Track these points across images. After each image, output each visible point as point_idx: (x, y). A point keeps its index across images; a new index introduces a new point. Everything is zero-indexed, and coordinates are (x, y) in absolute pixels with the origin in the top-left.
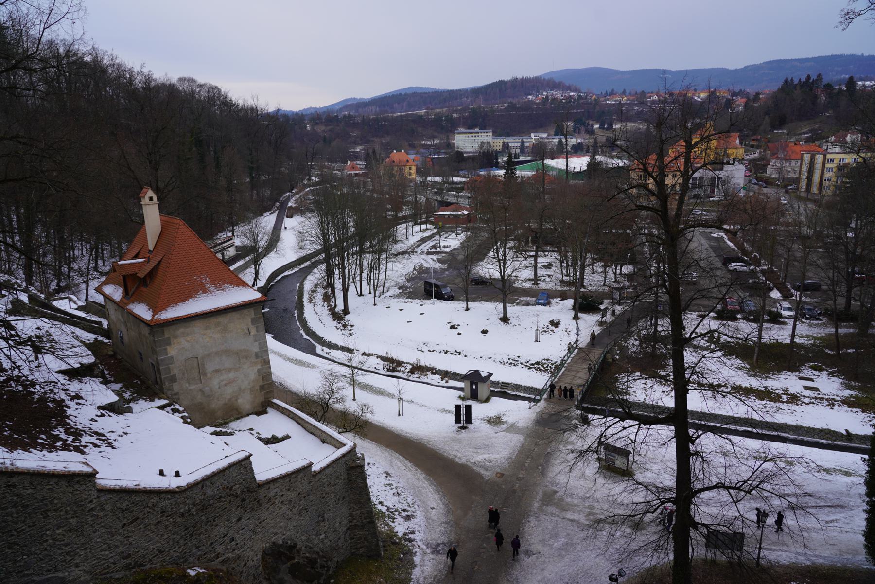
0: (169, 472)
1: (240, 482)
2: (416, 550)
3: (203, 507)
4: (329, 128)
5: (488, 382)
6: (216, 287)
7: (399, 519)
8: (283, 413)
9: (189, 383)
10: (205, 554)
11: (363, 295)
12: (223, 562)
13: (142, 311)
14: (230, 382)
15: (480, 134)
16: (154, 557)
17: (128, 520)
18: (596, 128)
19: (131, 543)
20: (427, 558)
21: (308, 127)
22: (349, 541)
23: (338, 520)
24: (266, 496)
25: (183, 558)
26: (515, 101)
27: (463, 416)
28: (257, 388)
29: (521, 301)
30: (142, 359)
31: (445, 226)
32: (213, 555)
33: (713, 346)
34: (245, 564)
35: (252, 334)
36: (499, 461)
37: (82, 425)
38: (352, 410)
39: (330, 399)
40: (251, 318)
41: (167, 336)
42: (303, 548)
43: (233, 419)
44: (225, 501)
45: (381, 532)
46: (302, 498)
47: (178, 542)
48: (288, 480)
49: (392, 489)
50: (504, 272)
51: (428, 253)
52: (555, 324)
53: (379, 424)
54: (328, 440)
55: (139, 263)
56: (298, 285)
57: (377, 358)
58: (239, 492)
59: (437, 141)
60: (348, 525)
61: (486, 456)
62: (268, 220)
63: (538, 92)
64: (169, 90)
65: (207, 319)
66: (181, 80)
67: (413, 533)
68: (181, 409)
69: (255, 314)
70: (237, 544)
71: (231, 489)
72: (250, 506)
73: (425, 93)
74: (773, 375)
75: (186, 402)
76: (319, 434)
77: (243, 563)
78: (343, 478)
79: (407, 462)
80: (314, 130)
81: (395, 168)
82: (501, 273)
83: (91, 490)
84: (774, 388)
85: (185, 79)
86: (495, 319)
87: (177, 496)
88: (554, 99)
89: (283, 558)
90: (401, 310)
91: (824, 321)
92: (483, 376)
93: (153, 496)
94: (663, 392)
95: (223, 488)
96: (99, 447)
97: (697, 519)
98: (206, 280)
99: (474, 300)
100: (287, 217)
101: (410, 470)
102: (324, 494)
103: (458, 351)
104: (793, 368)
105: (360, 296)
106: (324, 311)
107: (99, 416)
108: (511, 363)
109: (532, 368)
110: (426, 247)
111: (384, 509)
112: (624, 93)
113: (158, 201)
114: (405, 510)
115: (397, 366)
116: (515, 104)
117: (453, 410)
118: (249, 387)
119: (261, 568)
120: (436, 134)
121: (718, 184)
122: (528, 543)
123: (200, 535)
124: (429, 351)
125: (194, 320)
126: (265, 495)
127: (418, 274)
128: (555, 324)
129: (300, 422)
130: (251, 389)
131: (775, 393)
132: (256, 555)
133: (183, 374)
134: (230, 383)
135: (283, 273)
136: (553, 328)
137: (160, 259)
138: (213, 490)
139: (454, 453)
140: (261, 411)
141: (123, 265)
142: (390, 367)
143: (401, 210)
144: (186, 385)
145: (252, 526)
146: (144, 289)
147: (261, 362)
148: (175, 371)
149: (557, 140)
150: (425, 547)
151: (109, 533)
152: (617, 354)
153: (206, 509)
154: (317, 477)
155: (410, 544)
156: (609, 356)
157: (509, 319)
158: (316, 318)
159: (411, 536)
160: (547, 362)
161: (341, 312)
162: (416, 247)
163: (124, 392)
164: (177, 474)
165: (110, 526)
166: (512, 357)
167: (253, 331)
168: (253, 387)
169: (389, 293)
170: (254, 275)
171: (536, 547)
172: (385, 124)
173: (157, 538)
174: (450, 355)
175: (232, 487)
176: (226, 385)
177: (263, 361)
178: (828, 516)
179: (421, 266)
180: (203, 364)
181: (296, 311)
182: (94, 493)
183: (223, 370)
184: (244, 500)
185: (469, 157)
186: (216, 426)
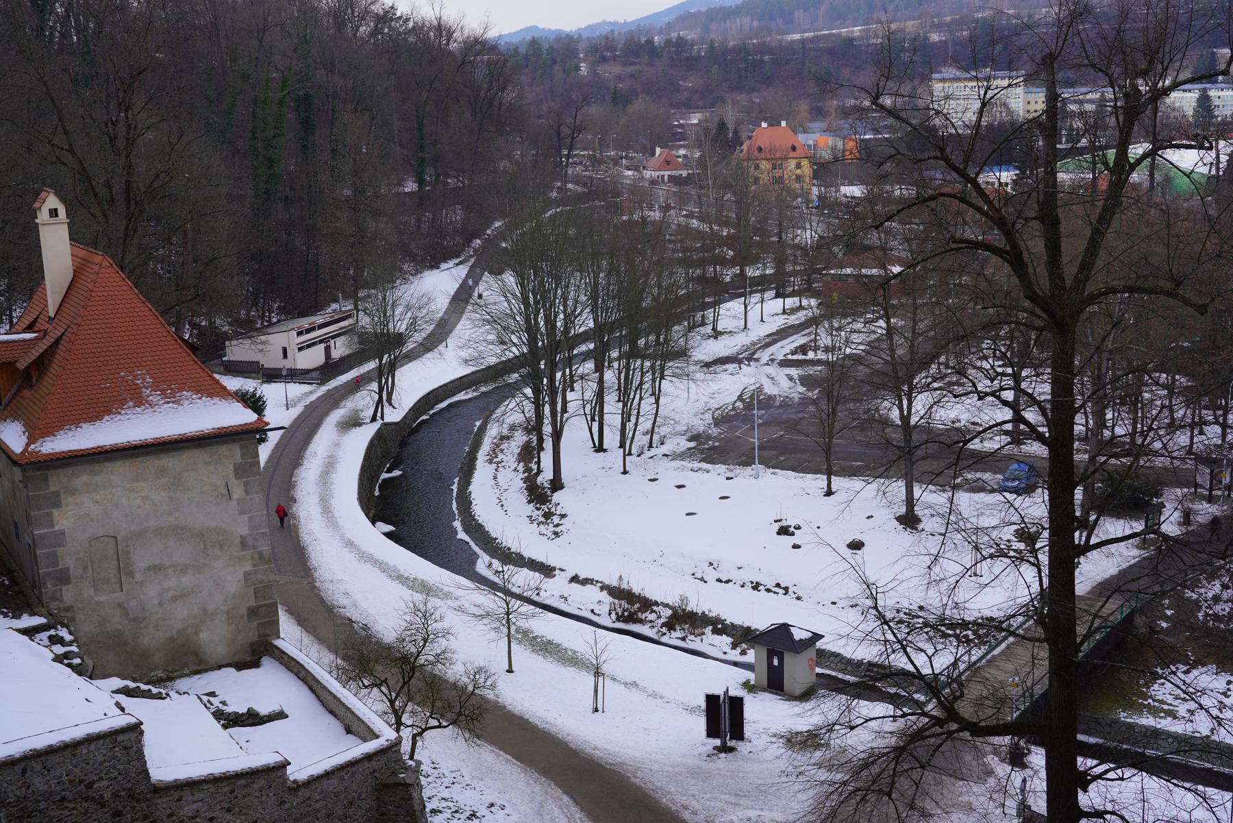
1: (113, 776)
4: (630, 69)
5: (810, 653)
6: (163, 392)
8: (289, 669)
9: (96, 590)
11: (605, 451)
14: (183, 595)
21: (584, 69)
24: (171, 815)
28: (243, 611)
35: (235, 497)
39: (419, 653)
40: (235, 465)
41: (53, 488)
43: (186, 671)
44: (73, 809)
48: (227, 789)
51: (785, 363)
53: (541, 725)
54: (354, 728)
55: (25, 341)
56: (478, 423)
57: (602, 589)
58: (107, 796)
65: (140, 459)
68: (68, 638)
69: (242, 456)
71: (90, 786)
75: (87, 627)
76: (342, 713)
79: (574, 809)
86: (886, 517)
90: (679, 487)
95: (71, 782)
98: (144, 379)
99: (851, 473)
103: (783, 586)
105: (597, 451)
106: (513, 480)
109: (948, 636)
110: (783, 349)
115: (640, 610)
117: (704, 706)
118: (225, 608)
124: (719, 580)
125: (111, 460)
126: (169, 811)
127: (745, 408)
129: (314, 687)
130: (228, 612)
133: (85, 569)
134: (184, 595)
135: (454, 394)
137: (59, 334)
138: (47, 782)
139: (684, 800)
140: (248, 660)
142: (624, 610)
143: (753, 261)
144: (88, 592)
146: (27, 393)
147: (252, 558)
148: (68, 562)
153: (29, 816)
154: (300, 794)
156: (1139, 620)
157: (920, 521)
161: (547, 485)
162: (760, 348)
168: (233, 608)
169: (664, 449)
170: (376, 397)
172: (762, 61)
174: (763, 592)
175: (93, 782)
176: (174, 599)
177: (256, 556)
180: (128, 553)
181: (456, 480)
183: (169, 567)
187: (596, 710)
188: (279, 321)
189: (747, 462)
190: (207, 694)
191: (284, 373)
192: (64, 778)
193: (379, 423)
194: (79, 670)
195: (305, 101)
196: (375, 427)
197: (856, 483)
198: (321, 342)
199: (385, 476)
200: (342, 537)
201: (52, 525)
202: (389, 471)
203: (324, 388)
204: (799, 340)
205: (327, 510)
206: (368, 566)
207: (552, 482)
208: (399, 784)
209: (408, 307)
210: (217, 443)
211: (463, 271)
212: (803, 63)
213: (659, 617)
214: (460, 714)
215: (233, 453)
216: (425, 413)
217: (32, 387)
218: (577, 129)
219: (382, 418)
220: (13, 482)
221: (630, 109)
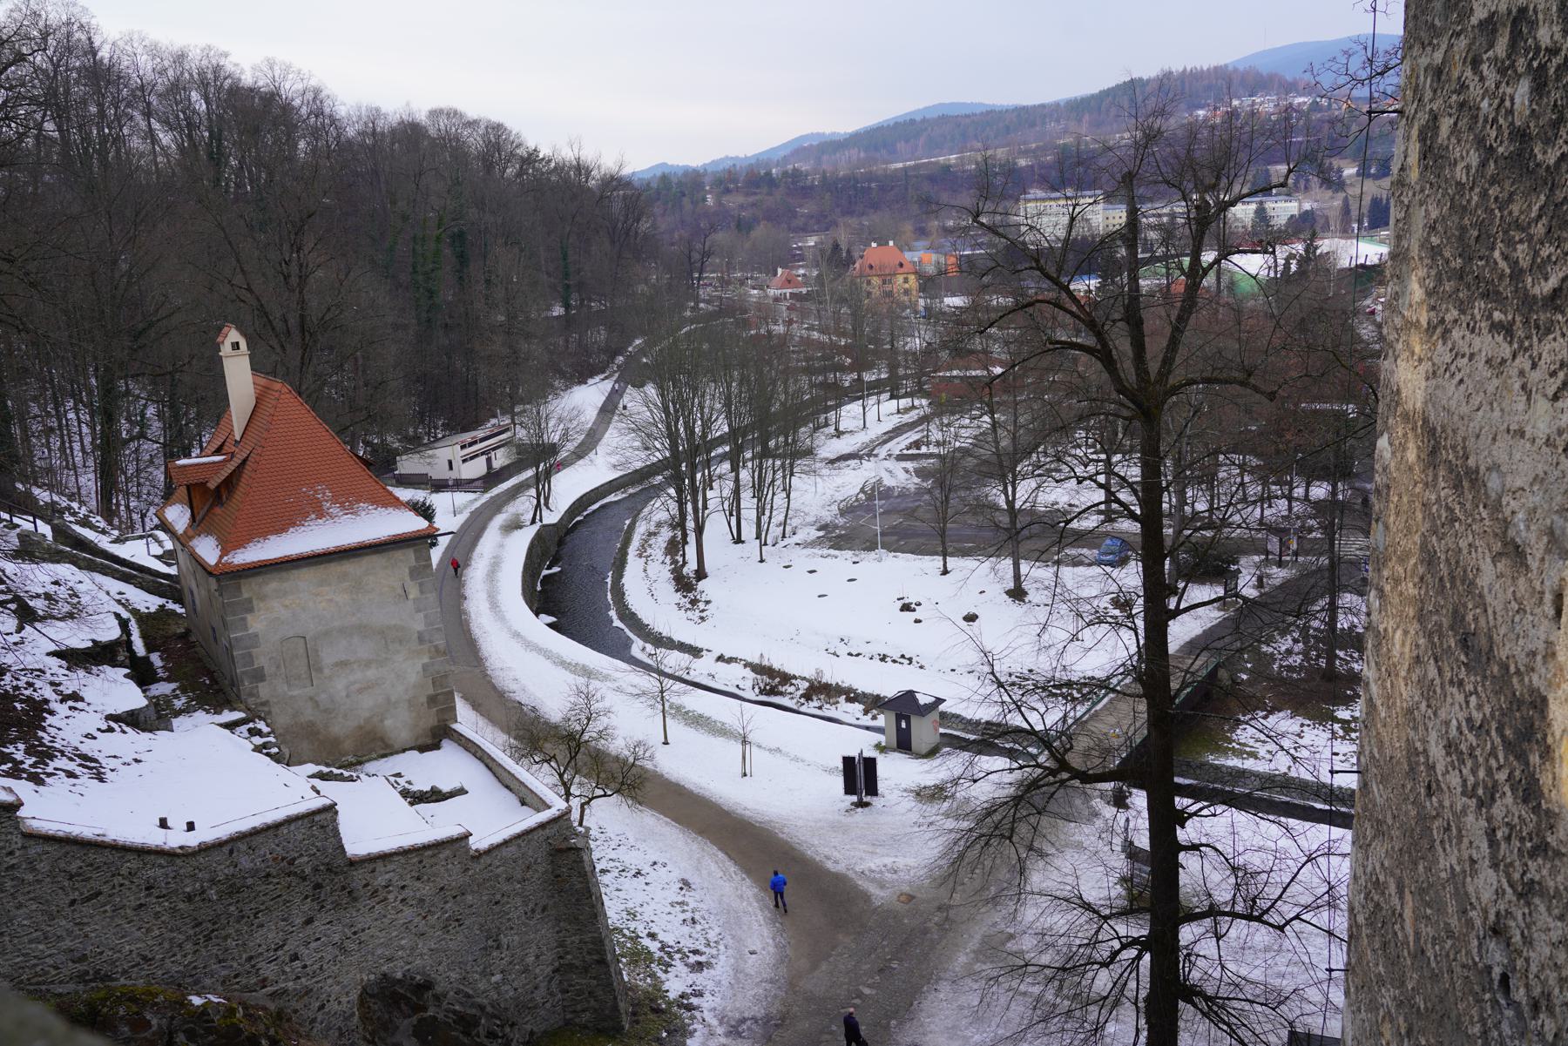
0: (174, 821)
2: (695, 1026)
3: (233, 889)
4: (751, 199)
5: (934, 716)
7: (679, 966)
9: (288, 683)
10: (236, 976)
11: (743, 542)
12: (273, 995)
13: (208, 550)
14: (368, 687)
16: (133, 967)
17: (82, 894)
18: (1350, 176)
19: (86, 936)
21: (710, 199)
23: (533, 950)
24: (366, 885)
25: (192, 976)
28: (423, 699)
31: (948, 403)
32: (253, 980)
34: (322, 1007)
37: (65, 743)
39: (583, 731)
41: (246, 595)
42: (452, 993)
43: (374, 755)
47: (180, 946)
48: (415, 860)
49: (683, 911)
51: (901, 458)
53: (696, 791)
55: (214, 463)
56: (627, 522)
57: (745, 666)
58: (307, 871)
60: (557, 964)
61: (888, 861)
62: (587, 398)
64: (410, 133)
66: (435, 114)
68: (266, 729)
69: (417, 559)
70: (305, 967)
72: (333, 899)
73: (967, 116)
75: (282, 720)
77: (317, 1004)
78: (541, 869)
81: (876, 281)
83: (11, 833)
87: (178, 861)
89: (404, 1007)
90: (811, 572)
93: (130, 856)
95: (275, 859)
99: (965, 553)
101: (731, 879)
102: (498, 897)
105: (736, 543)
106: (661, 571)
107: (103, 731)
110: (899, 445)
111: (653, 946)
113: (249, 349)
114: (696, 952)
117: (841, 766)
119: (356, 1019)
122: (921, 1030)
123: (226, 938)
124: (850, 654)
126: (364, 882)
127: (867, 499)
130: (409, 701)
132: (347, 993)
133: (278, 667)
134: (369, 687)
139: (826, 851)
141: (184, 466)
143: (869, 367)
145: (336, 938)
146: (218, 510)
148: (262, 661)
149: (1253, 206)
150: (715, 1022)
151: (44, 912)
152: (1245, 671)
155: (687, 1014)
156: (1223, 674)
157: (1026, 593)
158: (645, 585)
159: (695, 1001)
161: (692, 575)
163: (177, 697)
164: (191, 826)
165: (47, 901)
167: (414, 592)
169: (796, 539)
170: (535, 502)
172: (870, 188)
173: (139, 934)
175: (294, 859)
176: (360, 691)
180: (317, 651)
181: (610, 574)
182: (18, 841)
184: (318, 886)
187: (745, 775)
189: (871, 547)
190: (394, 775)
191: (450, 483)
194: (277, 759)
196: (536, 527)
197: (969, 563)
198: (483, 454)
199: (545, 572)
200: (509, 629)
201: (246, 629)
202: (548, 569)
203: (487, 496)
204: (913, 436)
205: (494, 605)
206: (534, 654)
207: (697, 572)
209: (560, 420)
210: (393, 549)
211: (608, 385)
212: (906, 189)
213: (798, 689)
214: (622, 783)
215: (408, 556)
216: (579, 515)
218: (706, 254)
219: (541, 520)
220: (209, 591)
221: (753, 234)
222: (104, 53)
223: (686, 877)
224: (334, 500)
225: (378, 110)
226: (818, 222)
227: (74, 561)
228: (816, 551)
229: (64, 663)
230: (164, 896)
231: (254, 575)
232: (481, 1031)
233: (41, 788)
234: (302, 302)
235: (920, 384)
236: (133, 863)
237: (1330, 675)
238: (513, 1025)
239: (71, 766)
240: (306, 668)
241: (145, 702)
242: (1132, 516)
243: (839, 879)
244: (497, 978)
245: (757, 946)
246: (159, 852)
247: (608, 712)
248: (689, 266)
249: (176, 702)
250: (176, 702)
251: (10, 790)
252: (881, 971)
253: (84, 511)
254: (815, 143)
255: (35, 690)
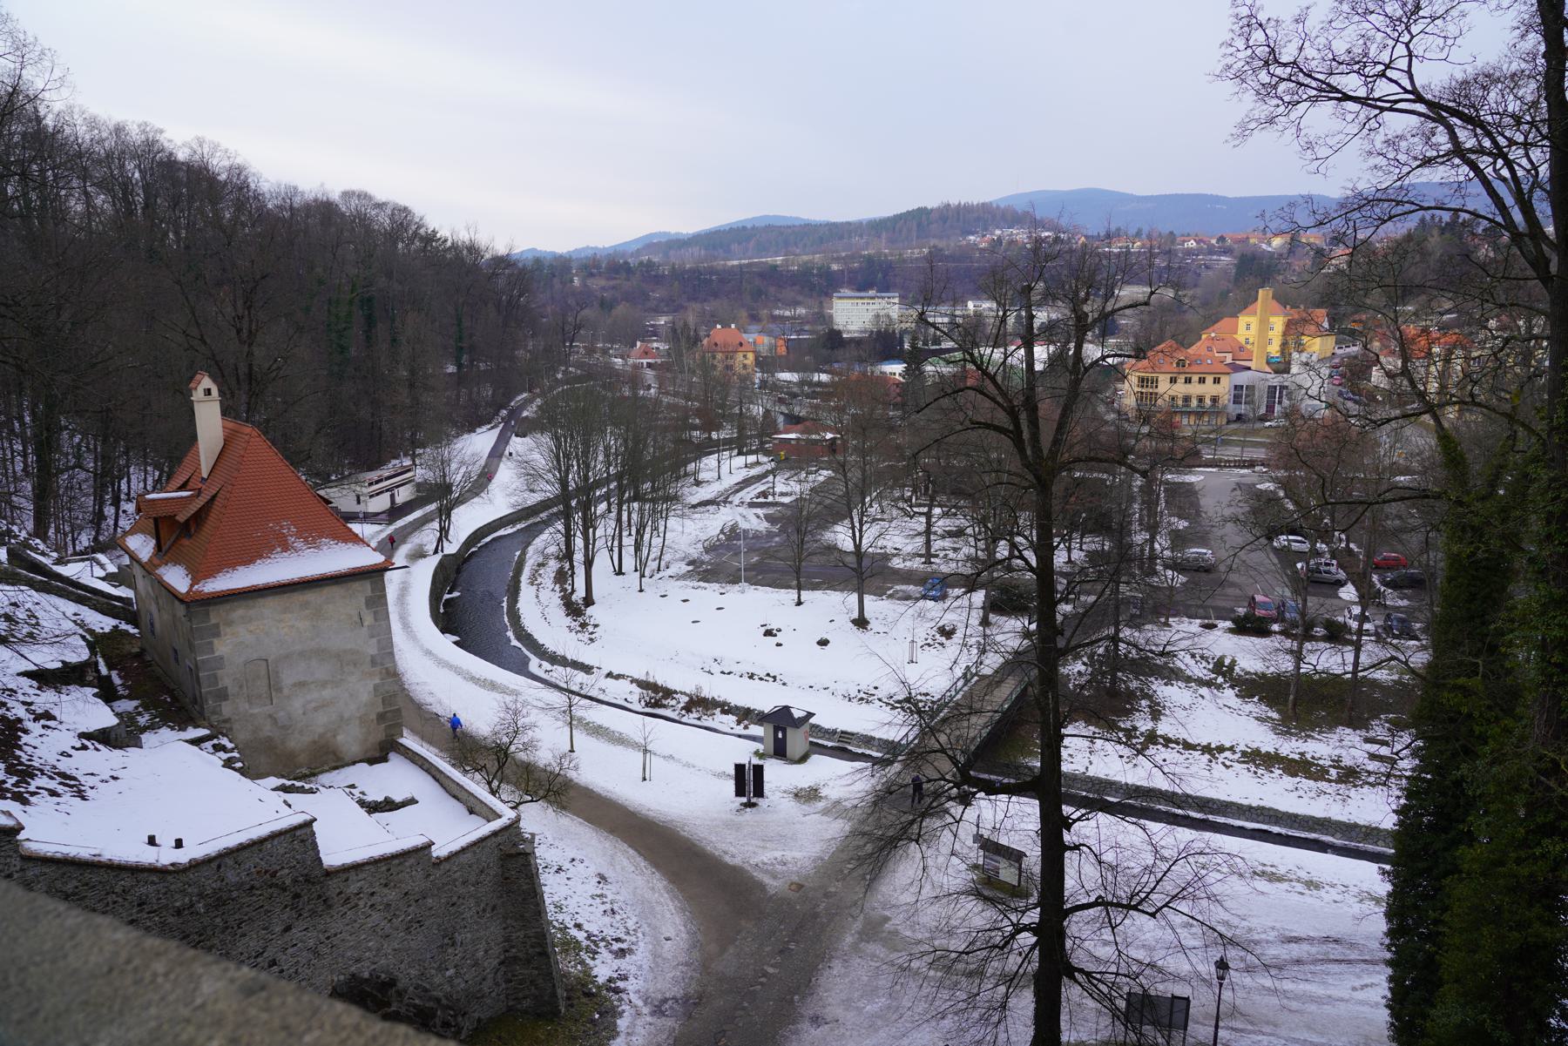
0: (166, 841)
3: (219, 902)
4: (612, 283)
5: (806, 727)
6: (306, 541)
7: (604, 954)
8: (413, 762)
9: (250, 703)
13: (177, 578)
14: (323, 706)
15: (877, 301)
20: (639, 1022)
22: (504, 986)
23: (483, 946)
24: (341, 893)
26: (941, 244)
27: (748, 782)
28: (374, 716)
29: (897, 591)
30: (177, 660)
31: (792, 459)
33: (1220, 680)
35: (366, 624)
36: (799, 864)
37: (42, 761)
38: (541, 764)
39: (511, 743)
41: (213, 621)
42: (411, 989)
43: (326, 768)
45: (567, 975)
46: (412, 902)
48: (384, 868)
49: (603, 903)
50: (861, 537)
51: (752, 505)
52: (947, 633)
54: (477, 809)
55: (182, 498)
56: (518, 553)
57: (632, 682)
58: (288, 882)
59: (801, 311)
61: (778, 854)
62: (480, 442)
63: (986, 229)
64: (324, 211)
66: (347, 195)
67: (624, 978)
68: (230, 745)
69: (372, 590)
70: (282, 971)
71: (274, 875)
73: (789, 227)
74: (1320, 732)
75: (243, 736)
79: (639, 859)
80: (585, 285)
81: (719, 356)
82: (854, 540)
83: (10, 856)
84: (1317, 756)
85: (353, 193)
87: (170, 878)
88: (1012, 242)
91: (1424, 642)
92: (796, 715)
93: (124, 875)
94: (1121, 757)
96: (58, 795)
97: (1075, 962)
98: (289, 529)
99: (815, 587)
100: (517, 436)
101: (642, 873)
102: (455, 899)
104: (1357, 722)
106: (552, 598)
108: (862, 699)
110: (749, 494)
111: (581, 936)
112: (1138, 234)
114: (618, 940)
115: (663, 697)
116: (941, 250)
117: (732, 772)
120: (800, 298)
121: (1280, 397)
122: (821, 1003)
124: (723, 673)
125: (263, 596)
128: (947, 633)
130: (360, 718)
131: (1318, 765)
133: (241, 687)
134: (323, 706)
136: (943, 639)
139: (724, 846)
140: (378, 756)
141: (153, 500)
143: (718, 428)
144: (244, 706)
145: (311, 943)
146: (186, 542)
148: (226, 681)
150: (640, 1003)
158: (537, 610)
159: (621, 984)
160: (923, 698)
161: (580, 602)
163: (140, 714)
164: (179, 844)
166: (863, 688)
169: (670, 572)
171: (834, 1010)
172: (711, 280)
175: (276, 872)
176: (316, 709)
178: (1359, 977)
179: (734, 528)
184: (297, 896)
185: (852, 340)
186: (283, 777)
187: (644, 779)
188: (350, 474)
189: (735, 580)
190: (349, 787)
191: (361, 516)
192: (253, 870)
193: (440, 555)
194: (243, 772)
195: (368, 302)
196: (439, 557)
197: (818, 594)
199: (447, 596)
200: (422, 647)
201: (213, 652)
202: (450, 593)
203: (392, 528)
204: (760, 487)
205: (406, 626)
208: (520, 854)
209: (462, 463)
211: (496, 433)
214: (549, 790)
215: (364, 588)
217: (191, 536)
218: (578, 327)
220: (174, 616)
221: (614, 312)
222: (49, 121)
223: (602, 872)
224: (299, 535)
225: (295, 188)
226: (667, 305)
227: (32, 585)
228: (687, 583)
229: (35, 684)
230: (155, 911)
231: (221, 603)
232: (437, 1020)
233: (27, 808)
234: (250, 354)
235: (762, 443)
236: (127, 882)
237: (1113, 693)
238: (463, 1015)
239: (52, 785)
240: (266, 689)
241: (115, 721)
242: (1031, 569)
243: (737, 871)
244: (451, 972)
245: (671, 933)
246: (152, 870)
247: (533, 726)
248: (567, 332)
249: (139, 719)
250: (139, 719)
251: (8, 814)
252: (781, 952)
253: (24, 534)
254: (663, 240)
255: (8, 710)
